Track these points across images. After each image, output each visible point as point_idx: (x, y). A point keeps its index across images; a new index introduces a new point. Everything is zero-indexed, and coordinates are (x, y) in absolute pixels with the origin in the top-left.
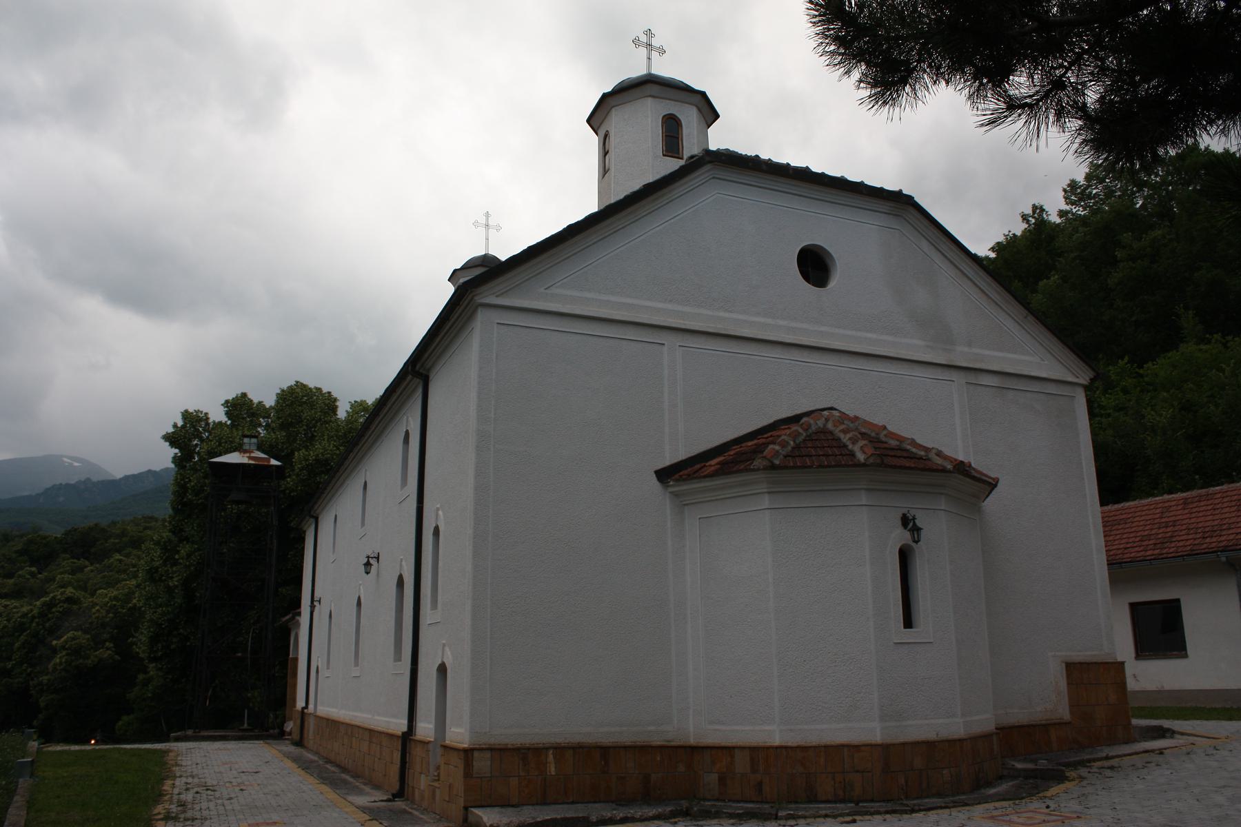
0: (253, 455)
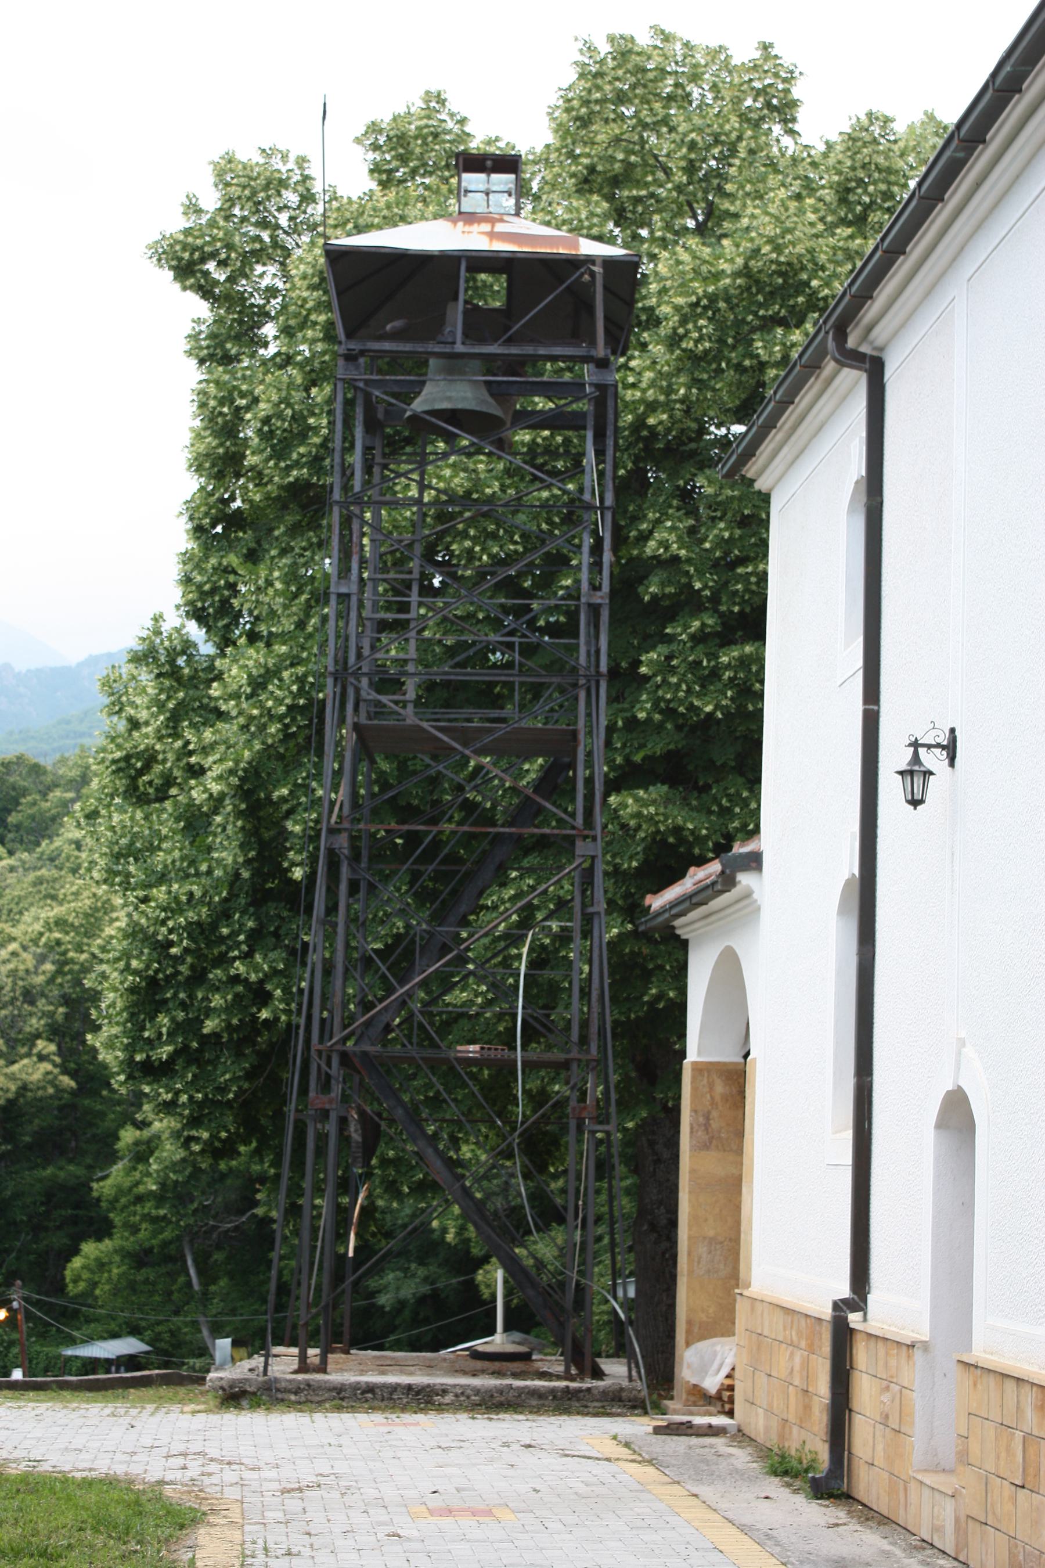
0: (500, 228)
